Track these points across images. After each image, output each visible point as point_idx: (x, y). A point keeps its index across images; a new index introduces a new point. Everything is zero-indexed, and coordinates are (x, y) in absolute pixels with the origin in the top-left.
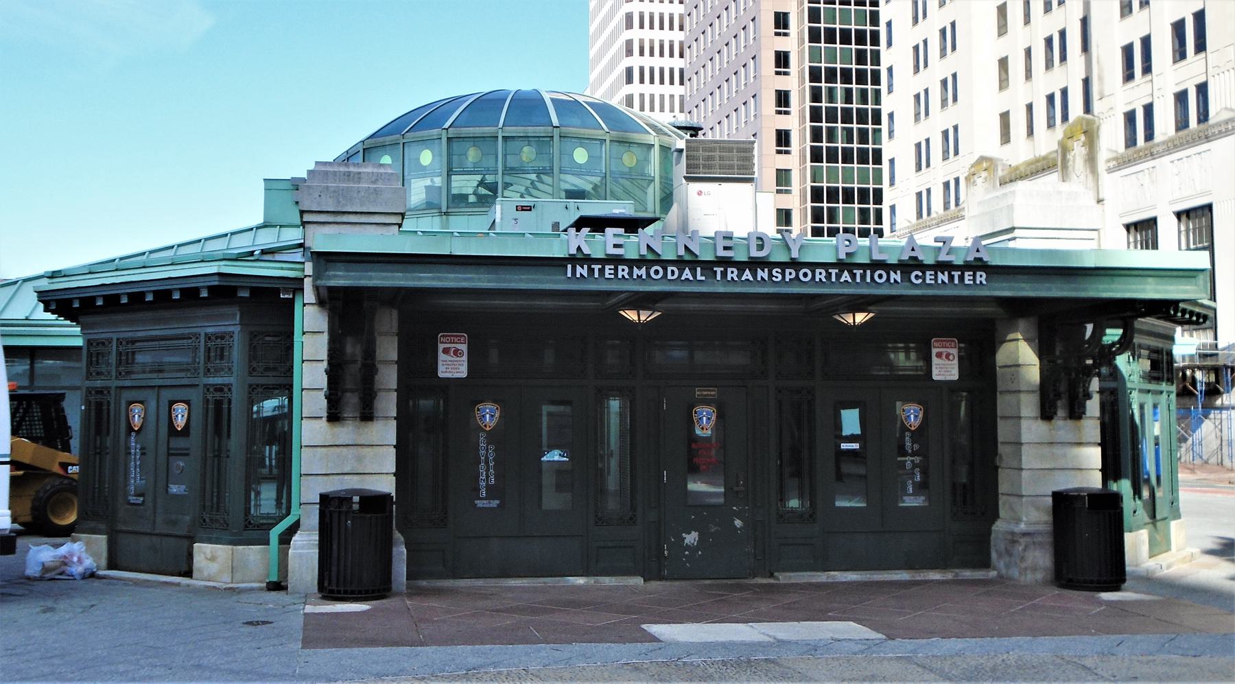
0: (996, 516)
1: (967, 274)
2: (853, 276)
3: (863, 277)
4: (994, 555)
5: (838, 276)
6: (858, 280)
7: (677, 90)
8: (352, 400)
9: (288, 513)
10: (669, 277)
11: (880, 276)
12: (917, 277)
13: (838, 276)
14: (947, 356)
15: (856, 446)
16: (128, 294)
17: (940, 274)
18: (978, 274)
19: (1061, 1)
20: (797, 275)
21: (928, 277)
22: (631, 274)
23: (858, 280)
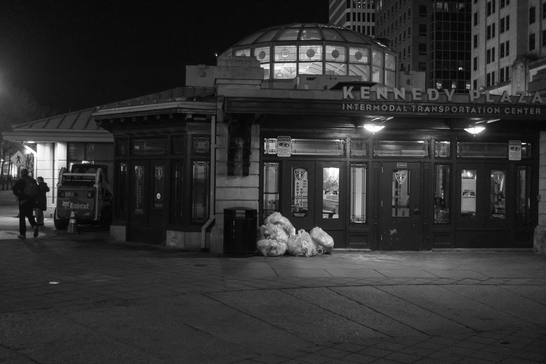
0: (536, 223)
1: (531, 109)
2: (477, 110)
3: (482, 110)
4: (535, 242)
5: (470, 110)
6: (479, 112)
7: (372, 24)
8: (239, 167)
9: (209, 218)
10: (390, 110)
11: (490, 110)
12: (507, 111)
13: (470, 110)
14: (516, 149)
15: (344, 108)
16: (136, 117)
17: (518, 110)
18: (537, 109)
19: (476, 1)
20: (451, 109)
21: (513, 111)
22: (372, 108)
23: (479, 112)
